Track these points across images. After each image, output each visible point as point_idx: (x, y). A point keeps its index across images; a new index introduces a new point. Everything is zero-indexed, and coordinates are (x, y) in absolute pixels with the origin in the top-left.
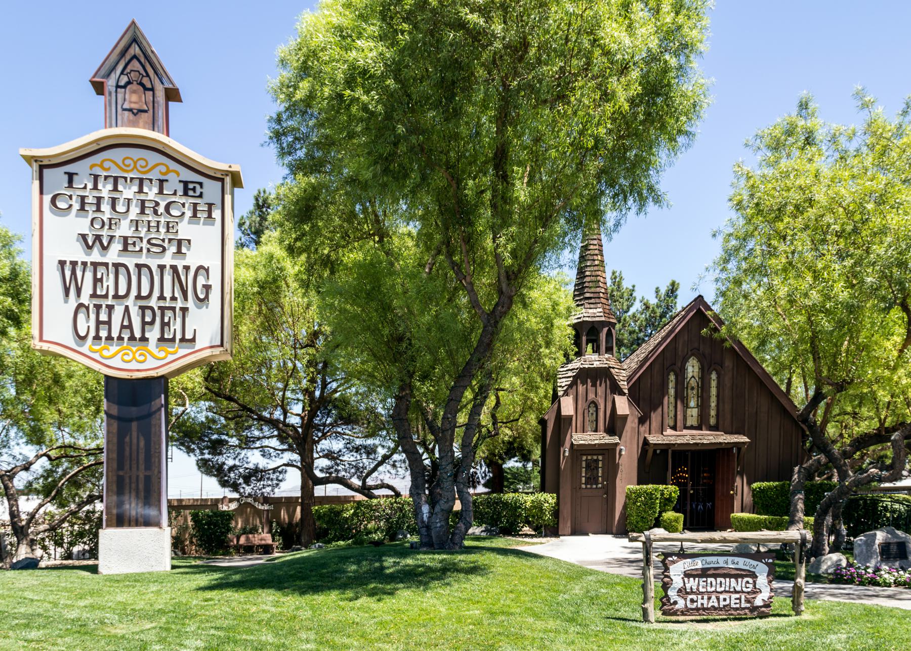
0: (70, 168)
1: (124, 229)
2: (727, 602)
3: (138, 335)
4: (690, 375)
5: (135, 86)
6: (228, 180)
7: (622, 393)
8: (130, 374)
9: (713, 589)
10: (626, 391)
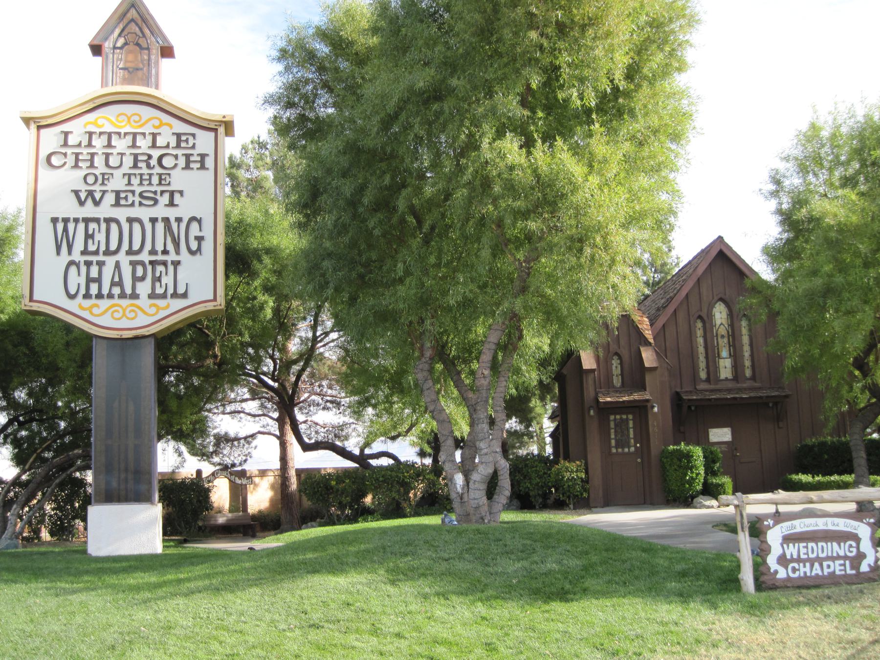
0: (65, 127)
1: (117, 183)
2: (831, 570)
3: (128, 291)
4: (718, 322)
5: (131, 47)
6: (221, 130)
7: (647, 343)
8: (120, 333)
9: (815, 555)
10: (652, 341)
